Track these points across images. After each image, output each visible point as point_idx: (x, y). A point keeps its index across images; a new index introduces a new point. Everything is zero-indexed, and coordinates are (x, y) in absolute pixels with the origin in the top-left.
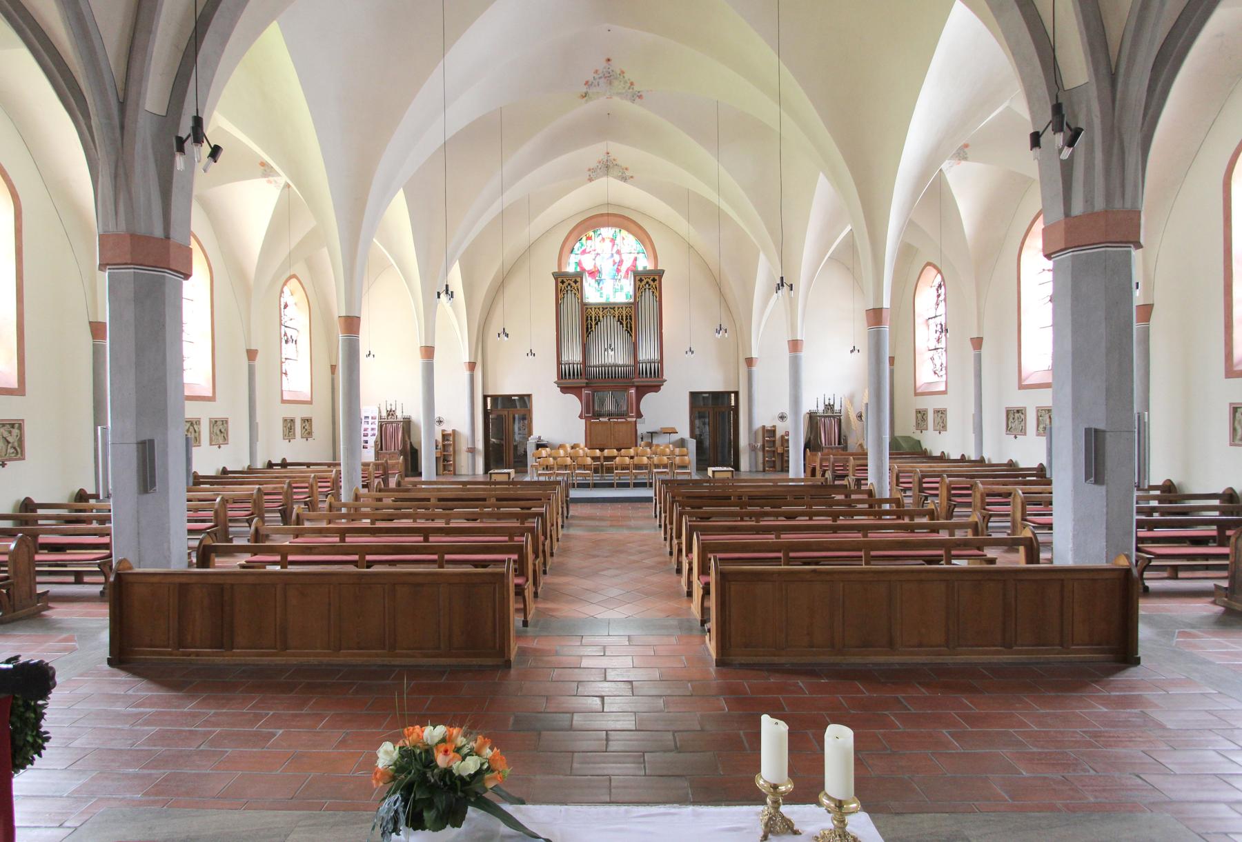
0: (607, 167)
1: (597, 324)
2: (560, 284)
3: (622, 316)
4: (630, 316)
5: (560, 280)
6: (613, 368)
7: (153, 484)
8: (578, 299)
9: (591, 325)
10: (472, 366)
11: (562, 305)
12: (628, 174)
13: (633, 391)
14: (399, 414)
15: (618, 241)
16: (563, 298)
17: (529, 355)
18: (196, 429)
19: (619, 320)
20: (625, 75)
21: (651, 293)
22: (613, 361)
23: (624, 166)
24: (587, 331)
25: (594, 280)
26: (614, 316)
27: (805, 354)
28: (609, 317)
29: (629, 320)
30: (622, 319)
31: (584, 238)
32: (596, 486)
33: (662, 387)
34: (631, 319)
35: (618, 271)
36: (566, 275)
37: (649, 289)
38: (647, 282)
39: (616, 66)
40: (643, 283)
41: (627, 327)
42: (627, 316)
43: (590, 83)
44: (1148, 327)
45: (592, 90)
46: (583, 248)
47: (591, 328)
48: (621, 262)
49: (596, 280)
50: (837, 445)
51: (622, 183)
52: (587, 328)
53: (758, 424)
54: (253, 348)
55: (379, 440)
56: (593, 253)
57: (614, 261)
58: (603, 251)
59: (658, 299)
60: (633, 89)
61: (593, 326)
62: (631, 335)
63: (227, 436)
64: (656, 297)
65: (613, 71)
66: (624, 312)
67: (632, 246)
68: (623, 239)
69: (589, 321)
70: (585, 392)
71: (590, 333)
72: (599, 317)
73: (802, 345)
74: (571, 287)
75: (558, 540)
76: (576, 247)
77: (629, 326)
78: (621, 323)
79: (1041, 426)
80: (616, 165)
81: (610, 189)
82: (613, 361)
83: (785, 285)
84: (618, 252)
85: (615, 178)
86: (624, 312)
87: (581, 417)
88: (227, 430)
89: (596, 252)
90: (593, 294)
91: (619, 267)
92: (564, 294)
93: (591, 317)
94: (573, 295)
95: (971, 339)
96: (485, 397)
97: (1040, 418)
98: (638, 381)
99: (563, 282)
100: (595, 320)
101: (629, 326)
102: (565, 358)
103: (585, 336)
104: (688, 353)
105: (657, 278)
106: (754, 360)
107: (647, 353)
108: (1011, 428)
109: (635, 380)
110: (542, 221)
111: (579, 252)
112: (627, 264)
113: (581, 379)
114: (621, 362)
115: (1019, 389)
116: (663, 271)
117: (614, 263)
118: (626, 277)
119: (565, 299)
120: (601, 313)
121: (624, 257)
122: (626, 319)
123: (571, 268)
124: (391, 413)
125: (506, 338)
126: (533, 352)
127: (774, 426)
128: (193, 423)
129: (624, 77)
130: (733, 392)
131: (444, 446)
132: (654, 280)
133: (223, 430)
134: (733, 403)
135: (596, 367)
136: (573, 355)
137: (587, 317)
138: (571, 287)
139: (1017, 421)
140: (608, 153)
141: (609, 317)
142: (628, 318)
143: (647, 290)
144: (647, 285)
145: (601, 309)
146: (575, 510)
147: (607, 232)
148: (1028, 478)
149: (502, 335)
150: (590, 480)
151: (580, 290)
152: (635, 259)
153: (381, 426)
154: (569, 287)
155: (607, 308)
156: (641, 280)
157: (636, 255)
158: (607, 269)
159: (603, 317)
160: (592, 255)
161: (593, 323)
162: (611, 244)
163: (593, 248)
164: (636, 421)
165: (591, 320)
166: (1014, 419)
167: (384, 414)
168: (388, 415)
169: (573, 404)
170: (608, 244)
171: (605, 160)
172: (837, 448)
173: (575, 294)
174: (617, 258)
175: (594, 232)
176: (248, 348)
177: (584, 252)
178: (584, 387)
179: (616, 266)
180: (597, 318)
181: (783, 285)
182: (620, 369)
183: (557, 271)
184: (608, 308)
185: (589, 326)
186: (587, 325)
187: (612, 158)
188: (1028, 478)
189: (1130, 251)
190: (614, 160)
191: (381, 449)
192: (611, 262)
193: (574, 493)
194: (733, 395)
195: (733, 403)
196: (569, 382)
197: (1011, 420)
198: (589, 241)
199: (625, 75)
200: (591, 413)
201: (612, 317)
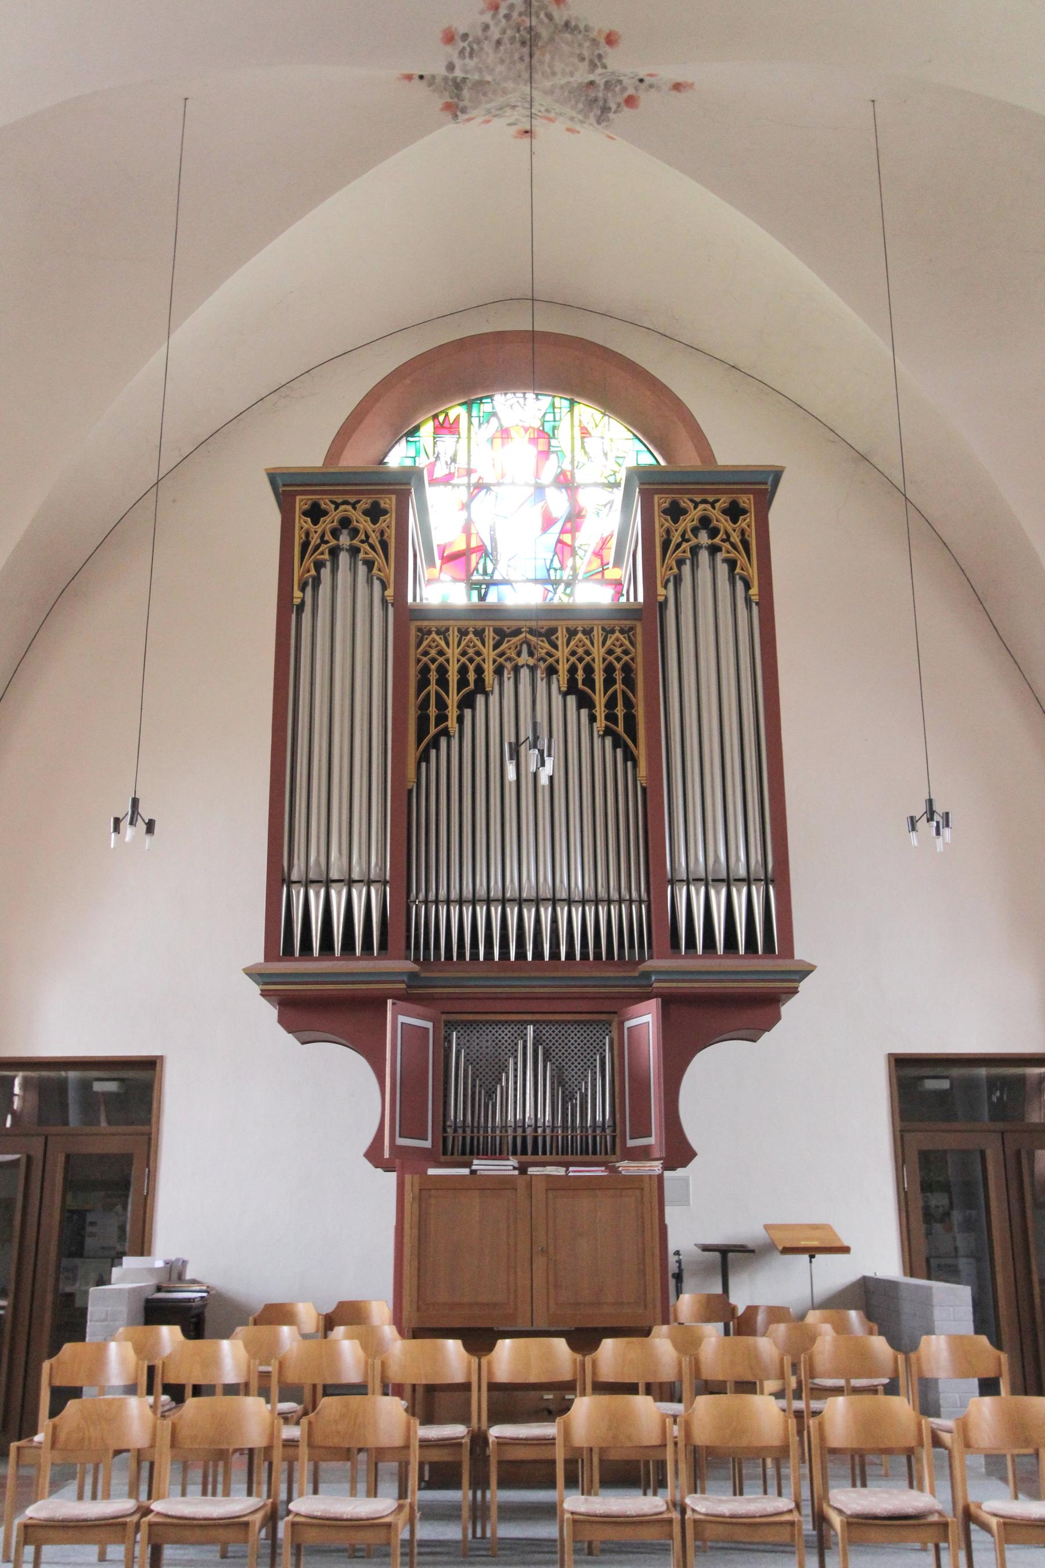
1: (467, 702)
15: (563, 439)
19: (572, 688)
21: (723, 569)
38: (705, 522)
41: (611, 718)
42: (609, 670)
47: (442, 718)
52: (423, 721)
59: (754, 591)
61: (452, 713)
64: (747, 586)
77: (620, 711)
78: (585, 702)
84: (565, 482)
101: (620, 711)
105: (746, 501)
117: (548, 522)
132: (734, 512)
154: (344, 540)
162: (532, 451)
174: (559, 503)
186: (424, 705)
198: (447, 442)
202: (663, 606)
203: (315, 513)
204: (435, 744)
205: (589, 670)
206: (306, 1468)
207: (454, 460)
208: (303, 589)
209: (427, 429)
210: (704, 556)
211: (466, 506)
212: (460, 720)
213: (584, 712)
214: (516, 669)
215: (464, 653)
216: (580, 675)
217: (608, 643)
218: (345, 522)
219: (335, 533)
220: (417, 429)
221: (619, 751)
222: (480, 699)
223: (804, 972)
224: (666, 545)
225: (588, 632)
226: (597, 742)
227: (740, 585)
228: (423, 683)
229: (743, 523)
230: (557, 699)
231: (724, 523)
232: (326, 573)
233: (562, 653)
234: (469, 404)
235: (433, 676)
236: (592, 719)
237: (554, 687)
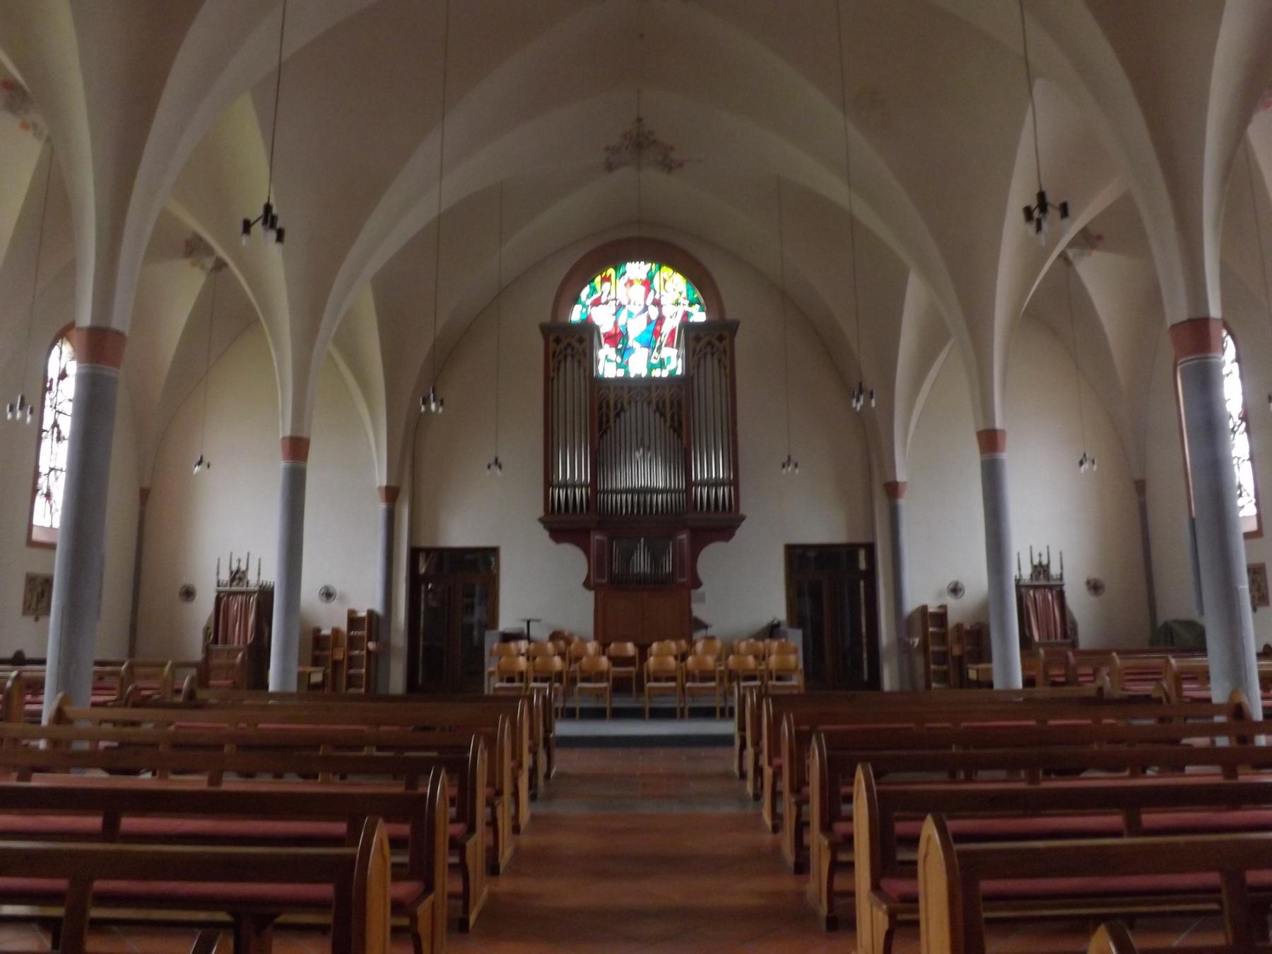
1: (618, 415)
5: (552, 338)
8: (585, 370)
10: (391, 494)
13: (684, 536)
14: (252, 578)
15: (656, 283)
19: (657, 409)
21: (716, 362)
24: (600, 428)
25: (614, 349)
26: (649, 403)
28: (639, 405)
32: (619, 714)
35: (657, 333)
38: (709, 343)
41: (672, 420)
42: (672, 403)
46: (595, 297)
47: (608, 421)
48: (661, 320)
49: (618, 351)
50: (1059, 640)
52: (601, 424)
53: (911, 603)
55: (212, 625)
56: (612, 303)
57: (649, 317)
59: (728, 371)
61: (612, 421)
64: (725, 370)
67: (681, 293)
70: (596, 537)
75: (516, 829)
77: (676, 418)
78: (663, 415)
84: (657, 303)
87: (587, 584)
91: (658, 328)
94: (576, 364)
96: (414, 553)
101: (676, 418)
105: (726, 334)
106: (900, 485)
111: (589, 302)
112: (671, 323)
114: (661, 485)
117: (649, 321)
122: (671, 408)
124: (238, 576)
127: (944, 607)
128: (557, 710)
131: (351, 639)
132: (721, 339)
134: (863, 565)
141: (639, 405)
144: (709, 349)
146: (565, 761)
147: (637, 270)
148: (407, 754)
149: (258, 228)
150: (606, 704)
153: (218, 600)
154: (569, 351)
158: (636, 327)
160: (611, 307)
162: (643, 289)
163: (612, 296)
167: (225, 577)
168: (232, 580)
169: (573, 561)
170: (639, 289)
172: (1061, 644)
174: (654, 313)
177: (597, 303)
179: (652, 327)
182: (660, 497)
185: (604, 419)
186: (601, 417)
188: (407, 754)
191: (216, 641)
192: (643, 318)
193: (563, 728)
194: (862, 554)
195: (863, 565)
198: (607, 285)
201: (645, 405)
202: (693, 378)
203: (558, 341)
204: (605, 432)
205: (664, 402)
206: (426, 821)
207: (609, 293)
208: (554, 371)
209: (598, 279)
210: (709, 356)
211: (615, 314)
212: (615, 422)
213: (662, 419)
214: (636, 402)
215: (616, 396)
216: (661, 405)
217: (672, 391)
218: (569, 345)
219: (566, 349)
220: (594, 279)
221: (676, 435)
222: (622, 415)
223: (742, 518)
224: (694, 352)
225: (664, 387)
226: (667, 432)
227: (723, 371)
228: (600, 408)
229: (724, 343)
230: (652, 414)
231: (717, 343)
232: (562, 364)
233: (654, 395)
234: (616, 269)
235: (604, 406)
236: (665, 422)
237: (651, 409)
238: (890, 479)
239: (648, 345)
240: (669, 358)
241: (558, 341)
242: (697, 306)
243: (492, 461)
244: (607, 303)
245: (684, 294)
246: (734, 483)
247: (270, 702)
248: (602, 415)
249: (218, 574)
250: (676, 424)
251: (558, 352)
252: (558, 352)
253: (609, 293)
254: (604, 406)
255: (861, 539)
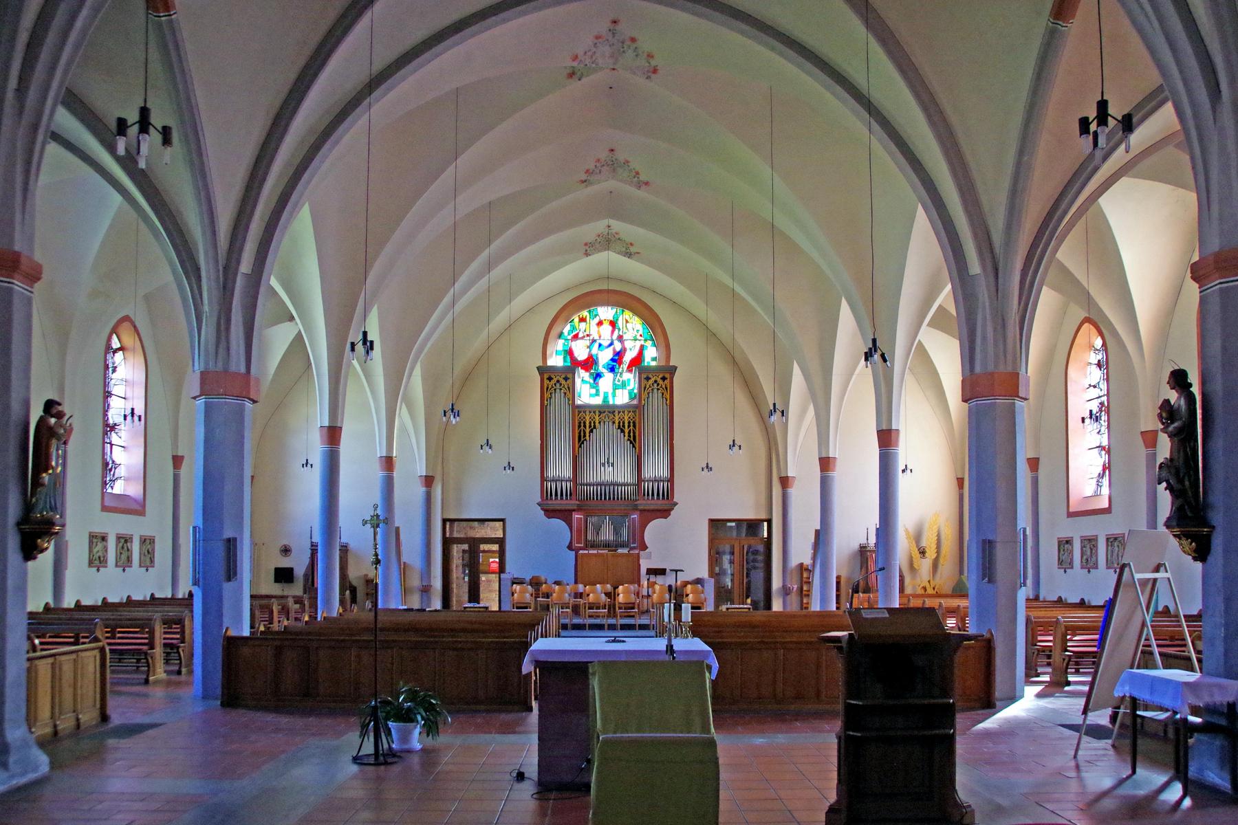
0: (607, 241)
1: (591, 431)
2: (546, 382)
3: (624, 423)
4: (634, 423)
5: (546, 376)
6: (612, 488)
7: (235, 574)
9: (585, 433)
11: (549, 406)
12: (633, 250)
15: (620, 323)
16: (550, 398)
17: (129, 418)
18: (129, 548)
19: (619, 427)
20: (629, 164)
22: (611, 478)
23: (628, 240)
26: (614, 423)
27: (837, 474)
29: (632, 427)
30: (624, 426)
31: (576, 320)
33: (672, 513)
34: (634, 426)
36: (553, 369)
37: (658, 389)
38: (656, 381)
39: (621, 156)
40: (651, 382)
41: (629, 436)
42: (629, 423)
43: (591, 171)
44: (1155, 453)
45: (592, 178)
47: (585, 436)
51: (625, 259)
54: (180, 454)
57: (614, 349)
58: (600, 337)
59: (668, 402)
60: (638, 178)
61: (587, 435)
62: (634, 446)
63: (154, 557)
65: (616, 159)
66: (626, 418)
68: (627, 322)
69: (582, 427)
71: (583, 443)
72: (594, 423)
73: (834, 463)
74: (561, 385)
76: (566, 331)
77: (632, 434)
78: (623, 431)
79: (1085, 557)
80: (619, 239)
81: (610, 260)
82: (611, 478)
83: (777, 410)
84: (620, 338)
85: (618, 253)
86: (626, 418)
88: (153, 550)
89: (591, 338)
90: (586, 393)
92: (551, 394)
93: (585, 423)
94: (563, 395)
95: (1028, 459)
97: (1084, 549)
98: (643, 503)
99: (550, 379)
100: (590, 426)
101: (632, 434)
102: (551, 473)
103: (577, 446)
104: (1087, 421)
105: (667, 376)
107: (655, 468)
108: (1062, 561)
109: (638, 502)
110: (522, 301)
111: (570, 337)
113: (570, 499)
114: (621, 480)
115: (1068, 517)
116: (675, 368)
118: (629, 369)
119: (553, 400)
120: (597, 418)
121: (628, 344)
122: (629, 426)
123: (556, 360)
125: (490, 451)
126: (512, 465)
129: (629, 166)
130: (764, 520)
132: (664, 379)
133: (150, 551)
135: (590, 485)
136: (561, 468)
137: (580, 423)
138: (561, 385)
139: (1066, 554)
140: (609, 227)
142: (632, 424)
143: (655, 390)
145: (597, 413)
147: (606, 313)
151: (571, 389)
152: (642, 348)
154: (558, 385)
155: (604, 412)
156: (648, 379)
157: (642, 343)
159: (600, 423)
161: (588, 430)
162: (610, 328)
164: (639, 553)
165: (585, 426)
166: (1064, 550)
170: (607, 328)
171: (606, 233)
173: (565, 393)
174: (618, 346)
175: (590, 312)
176: (174, 454)
177: (576, 337)
178: (574, 510)
180: (592, 424)
181: (775, 411)
183: (542, 365)
184: (606, 410)
186: (580, 433)
187: (614, 231)
189: (1014, 403)
190: (617, 233)
196: (556, 504)
197: (1062, 552)
198: (583, 324)
199: (629, 164)
200: (580, 543)
208: (547, 400)
212: (589, 436)
218: (558, 381)
222: (594, 430)
235: (582, 425)
236: (624, 436)
238: (783, 475)
239: (612, 370)
240: (629, 380)
241: (550, 379)
242: (650, 342)
243: (506, 465)
244: (583, 338)
245: (641, 332)
246: (671, 480)
247: (1191, 463)
248: (581, 431)
249: (311, 538)
250: (632, 439)
251: (550, 387)
252: (550, 387)
253: (585, 331)
254: (582, 425)
255: (763, 516)
